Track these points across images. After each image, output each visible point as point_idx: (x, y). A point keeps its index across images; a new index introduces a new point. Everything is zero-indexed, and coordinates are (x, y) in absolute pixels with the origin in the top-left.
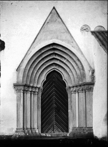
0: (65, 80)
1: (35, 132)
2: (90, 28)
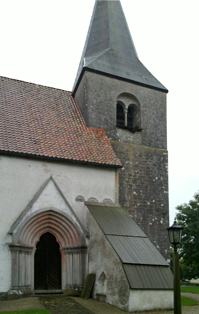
0: (59, 241)
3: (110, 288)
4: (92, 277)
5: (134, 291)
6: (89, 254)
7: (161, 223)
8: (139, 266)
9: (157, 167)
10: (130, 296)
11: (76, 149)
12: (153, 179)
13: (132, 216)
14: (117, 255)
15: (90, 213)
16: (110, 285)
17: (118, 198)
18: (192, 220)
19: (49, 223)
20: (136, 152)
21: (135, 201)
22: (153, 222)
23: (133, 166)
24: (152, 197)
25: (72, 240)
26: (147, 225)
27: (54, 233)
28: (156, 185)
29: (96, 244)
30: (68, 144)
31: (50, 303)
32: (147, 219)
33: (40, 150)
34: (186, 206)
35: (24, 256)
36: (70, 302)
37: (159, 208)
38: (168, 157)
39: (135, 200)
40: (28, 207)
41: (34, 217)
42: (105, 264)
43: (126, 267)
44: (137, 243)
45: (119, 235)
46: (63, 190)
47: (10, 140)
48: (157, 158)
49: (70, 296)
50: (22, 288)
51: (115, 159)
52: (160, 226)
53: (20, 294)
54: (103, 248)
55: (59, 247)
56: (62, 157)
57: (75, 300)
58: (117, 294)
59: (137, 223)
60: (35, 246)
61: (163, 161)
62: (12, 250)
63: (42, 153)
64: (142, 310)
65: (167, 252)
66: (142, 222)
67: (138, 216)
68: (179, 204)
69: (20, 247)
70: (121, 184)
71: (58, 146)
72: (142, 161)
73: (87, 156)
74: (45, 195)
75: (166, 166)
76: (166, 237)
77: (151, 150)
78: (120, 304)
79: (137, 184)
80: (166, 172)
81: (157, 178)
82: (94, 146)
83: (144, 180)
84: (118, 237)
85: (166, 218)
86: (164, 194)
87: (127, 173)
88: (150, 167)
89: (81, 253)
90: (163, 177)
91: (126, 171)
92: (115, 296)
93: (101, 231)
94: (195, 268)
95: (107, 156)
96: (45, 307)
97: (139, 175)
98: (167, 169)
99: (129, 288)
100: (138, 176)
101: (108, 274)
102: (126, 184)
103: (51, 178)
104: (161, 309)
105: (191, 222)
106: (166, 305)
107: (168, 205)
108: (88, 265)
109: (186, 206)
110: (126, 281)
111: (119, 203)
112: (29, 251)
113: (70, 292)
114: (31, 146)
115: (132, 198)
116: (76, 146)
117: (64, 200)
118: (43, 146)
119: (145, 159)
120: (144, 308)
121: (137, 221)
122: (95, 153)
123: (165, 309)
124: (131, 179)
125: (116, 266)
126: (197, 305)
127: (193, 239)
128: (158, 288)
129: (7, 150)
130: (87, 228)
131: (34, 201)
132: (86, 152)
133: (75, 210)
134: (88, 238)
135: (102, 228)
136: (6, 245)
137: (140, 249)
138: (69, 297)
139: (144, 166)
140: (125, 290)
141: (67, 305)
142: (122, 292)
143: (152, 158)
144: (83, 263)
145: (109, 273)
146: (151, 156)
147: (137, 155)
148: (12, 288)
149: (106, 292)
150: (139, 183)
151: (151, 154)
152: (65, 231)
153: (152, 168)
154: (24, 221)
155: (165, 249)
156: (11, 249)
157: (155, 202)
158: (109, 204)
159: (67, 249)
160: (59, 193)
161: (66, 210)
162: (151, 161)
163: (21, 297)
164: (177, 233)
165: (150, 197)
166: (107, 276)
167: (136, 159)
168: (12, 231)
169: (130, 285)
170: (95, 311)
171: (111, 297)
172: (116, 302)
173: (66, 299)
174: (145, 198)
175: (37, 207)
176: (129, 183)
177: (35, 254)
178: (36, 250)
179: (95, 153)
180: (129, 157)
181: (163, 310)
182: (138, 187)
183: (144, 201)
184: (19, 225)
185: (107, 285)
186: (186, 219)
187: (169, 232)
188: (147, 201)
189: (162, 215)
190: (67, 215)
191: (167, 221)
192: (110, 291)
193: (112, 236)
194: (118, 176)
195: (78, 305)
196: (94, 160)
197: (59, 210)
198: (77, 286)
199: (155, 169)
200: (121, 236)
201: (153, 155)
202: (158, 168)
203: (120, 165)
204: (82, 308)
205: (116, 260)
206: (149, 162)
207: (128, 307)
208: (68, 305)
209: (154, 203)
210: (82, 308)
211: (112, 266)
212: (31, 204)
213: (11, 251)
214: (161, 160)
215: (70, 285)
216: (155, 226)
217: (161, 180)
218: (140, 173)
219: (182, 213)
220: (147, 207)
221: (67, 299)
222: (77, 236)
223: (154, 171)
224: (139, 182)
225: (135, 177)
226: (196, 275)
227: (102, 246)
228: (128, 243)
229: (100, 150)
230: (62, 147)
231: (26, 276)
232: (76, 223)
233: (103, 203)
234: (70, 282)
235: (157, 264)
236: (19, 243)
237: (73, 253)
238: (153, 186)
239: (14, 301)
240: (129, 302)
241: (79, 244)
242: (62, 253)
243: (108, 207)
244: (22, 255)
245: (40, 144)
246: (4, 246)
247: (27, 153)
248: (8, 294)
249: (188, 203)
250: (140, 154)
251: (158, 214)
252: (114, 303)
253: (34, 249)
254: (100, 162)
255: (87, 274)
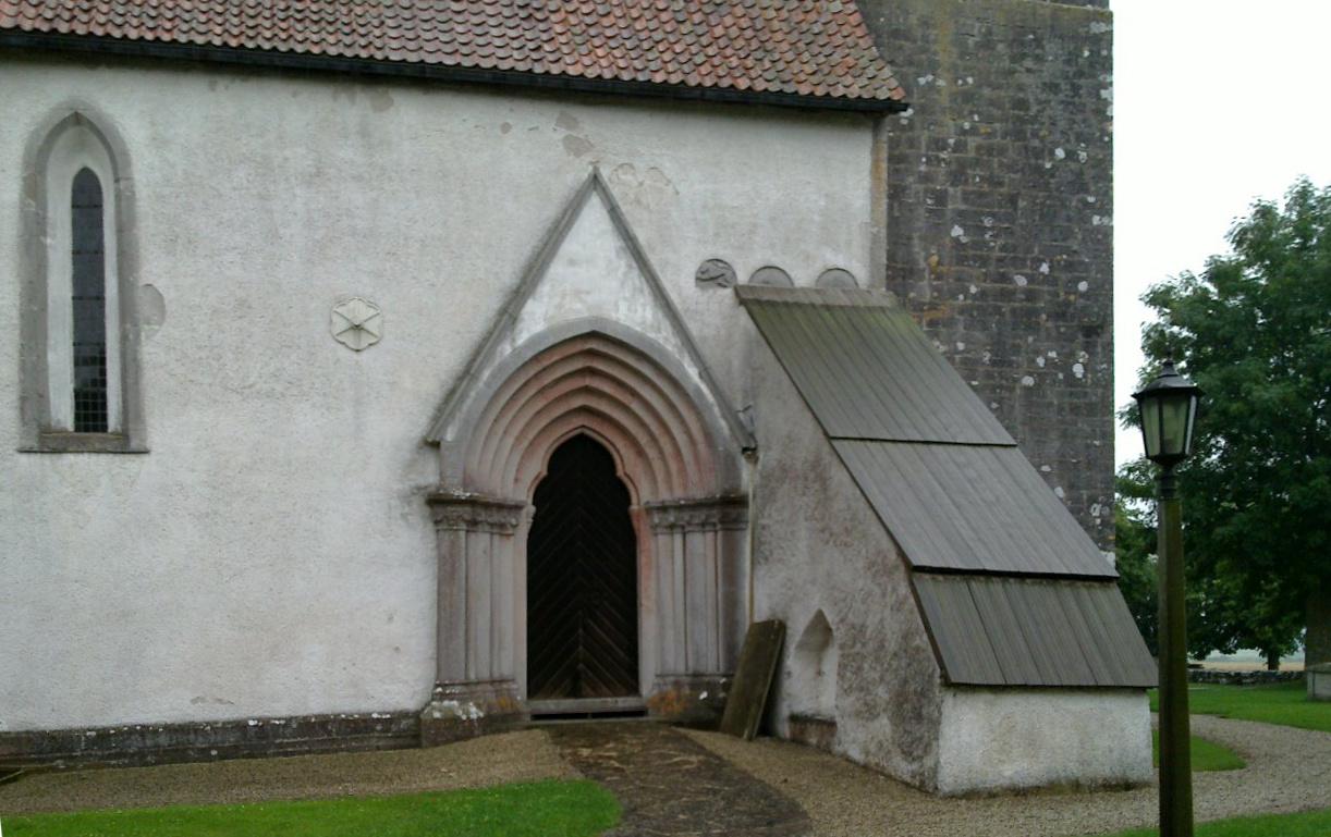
0: (626, 474)
1: (468, 718)
2: (734, 273)
3: (854, 686)
4: (772, 635)
5: (961, 697)
6: (757, 532)
7: (1073, 375)
8: (982, 578)
9: (1061, 96)
10: (944, 721)
11: (700, 30)
12: (1044, 159)
13: (943, 348)
14: (883, 532)
15: (760, 337)
16: (853, 673)
17: (885, 261)
18: (1215, 358)
19: (588, 390)
20: (964, 25)
21: (957, 272)
22: (1039, 374)
23: (953, 97)
24: (1036, 250)
25: (682, 470)
26: (1011, 390)
27: (609, 441)
28: (1057, 189)
29: (786, 486)
30: (665, 10)
31: (601, 757)
32: (1014, 358)
33: (547, 47)
34: (1190, 288)
35: (489, 543)
36: (684, 751)
37: (1070, 301)
38: (1112, 44)
39: (957, 268)
40: (502, 323)
41: (525, 365)
42: (829, 575)
43: (926, 584)
44: (972, 474)
45: (894, 441)
46: (642, 236)
47: (425, 10)
48: (1060, 52)
49: (680, 724)
50: (479, 688)
51: (871, 72)
52: (1069, 389)
53: (474, 716)
54: (818, 503)
55: (628, 501)
56: (641, 77)
57: (700, 741)
58: (884, 710)
59: (968, 378)
60: (528, 496)
61: (1091, 65)
62: (439, 519)
63: (557, 61)
64: (996, 787)
65: (1101, 516)
66: (989, 376)
67: (973, 343)
68: (1159, 279)
69: (471, 502)
70: (896, 193)
71: (622, 23)
72: (993, 70)
73: (749, 62)
74: (572, 263)
75: (1106, 88)
76: (1097, 443)
77: (1034, 14)
78: (899, 758)
79: (970, 188)
80: (1101, 122)
81: (1060, 153)
82: (778, 10)
83: (1001, 165)
84: (868, 448)
85: (1099, 349)
86: (1092, 232)
87: (924, 137)
88: (1031, 100)
89: (719, 527)
90: (1087, 147)
91: (918, 125)
92: (876, 724)
93: (810, 425)
94: (1226, 598)
95: (835, 56)
96: (582, 772)
97: (978, 140)
98: (1108, 103)
99: (938, 681)
100: (974, 144)
101: (842, 621)
102: (918, 192)
103: (595, 180)
104: (1082, 781)
105: (1214, 365)
106: (1103, 765)
107: (1107, 287)
108: (752, 578)
109: (1190, 288)
110: (924, 651)
111: (888, 289)
112: (508, 519)
113: (677, 708)
114: (513, 33)
115: (946, 261)
116: (697, 18)
117: (648, 281)
118: (559, 28)
119: (1005, 57)
120: (1004, 777)
121: (969, 368)
122: (785, 46)
123: (1100, 782)
124: (943, 165)
125: (879, 585)
126: (1242, 768)
127: (1220, 448)
128: (1066, 683)
129: (413, 58)
130: (746, 409)
131: (524, 293)
132: (743, 43)
133: (694, 328)
134: (749, 458)
135: (815, 410)
136: (413, 498)
137: (982, 500)
138: (673, 728)
139: (1003, 94)
140: (922, 694)
141: (669, 765)
142: (906, 701)
143: (1038, 51)
144: (730, 573)
145: (846, 615)
146: (1034, 44)
147: (971, 41)
148: (439, 690)
149: (837, 707)
150: (978, 179)
151: (1034, 33)
152: (654, 427)
153: (1040, 102)
154: (488, 385)
155: (1093, 500)
156: (433, 514)
157: (1051, 271)
158: (844, 291)
159: (663, 509)
160: (628, 252)
161: (659, 330)
162: (1035, 67)
163: (476, 732)
164: (1177, 415)
165: (1029, 250)
166: (838, 629)
167: (969, 63)
168: (439, 431)
169: (943, 667)
170: (793, 790)
171: (860, 729)
172: (880, 749)
173: (663, 737)
174: (1004, 254)
175: (539, 320)
176: (932, 186)
177: (531, 534)
178: (535, 517)
179: (785, 46)
180: (935, 53)
181: (1089, 787)
182: (973, 204)
183: (1002, 270)
184: (469, 402)
185: (839, 674)
186: (1188, 353)
187: (1144, 410)
188: (1012, 270)
189: (1081, 339)
190: (662, 351)
191: (1105, 366)
192: (852, 698)
193: (858, 442)
194: (884, 155)
195: (717, 762)
196: (777, 82)
197: (628, 327)
198: (706, 679)
199: (1052, 109)
200: (900, 445)
201: (1043, 39)
202: (1069, 100)
203: (896, 98)
204: (736, 778)
205: (879, 553)
206: (1026, 74)
207: (935, 770)
208: (676, 763)
209: (1046, 279)
210: (736, 778)
211: (860, 583)
212: (512, 307)
213: (437, 523)
214: (1080, 60)
215: (672, 675)
216: (1049, 392)
217: (1078, 161)
218: (982, 131)
219: (1173, 324)
220: (1015, 301)
221: (667, 739)
222: (702, 447)
223: (1050, 118)
224: (980, 177)
225: (961, 152)
226: (1231, 631)
227: (813, 494)
228: (929, 476)
229: (804, 26)
230: (638, 26)
231: (496, 635)
232: (698, 390)
233: (818, 291)
234: (677, 664)
235: (1065, 571)
236: (465, 486)
237: (688, 529)
238: (1041, 194)
239: (451, 750)
240: (938, 746)
241: (703, 486)
242: (642, 528)
243: (842, 307)
244: (481, 540)
245: (546, 19)
246: (406, 498)
247: (495, 67)
248: (422, 716)
249: (1199, 269)
250: (985, 35)
251: (1064, 334)
252: (874, 755)
253: (524, 511)
254: (804, 90)
255: (748, 624)
